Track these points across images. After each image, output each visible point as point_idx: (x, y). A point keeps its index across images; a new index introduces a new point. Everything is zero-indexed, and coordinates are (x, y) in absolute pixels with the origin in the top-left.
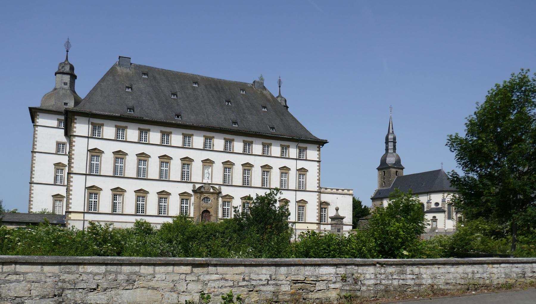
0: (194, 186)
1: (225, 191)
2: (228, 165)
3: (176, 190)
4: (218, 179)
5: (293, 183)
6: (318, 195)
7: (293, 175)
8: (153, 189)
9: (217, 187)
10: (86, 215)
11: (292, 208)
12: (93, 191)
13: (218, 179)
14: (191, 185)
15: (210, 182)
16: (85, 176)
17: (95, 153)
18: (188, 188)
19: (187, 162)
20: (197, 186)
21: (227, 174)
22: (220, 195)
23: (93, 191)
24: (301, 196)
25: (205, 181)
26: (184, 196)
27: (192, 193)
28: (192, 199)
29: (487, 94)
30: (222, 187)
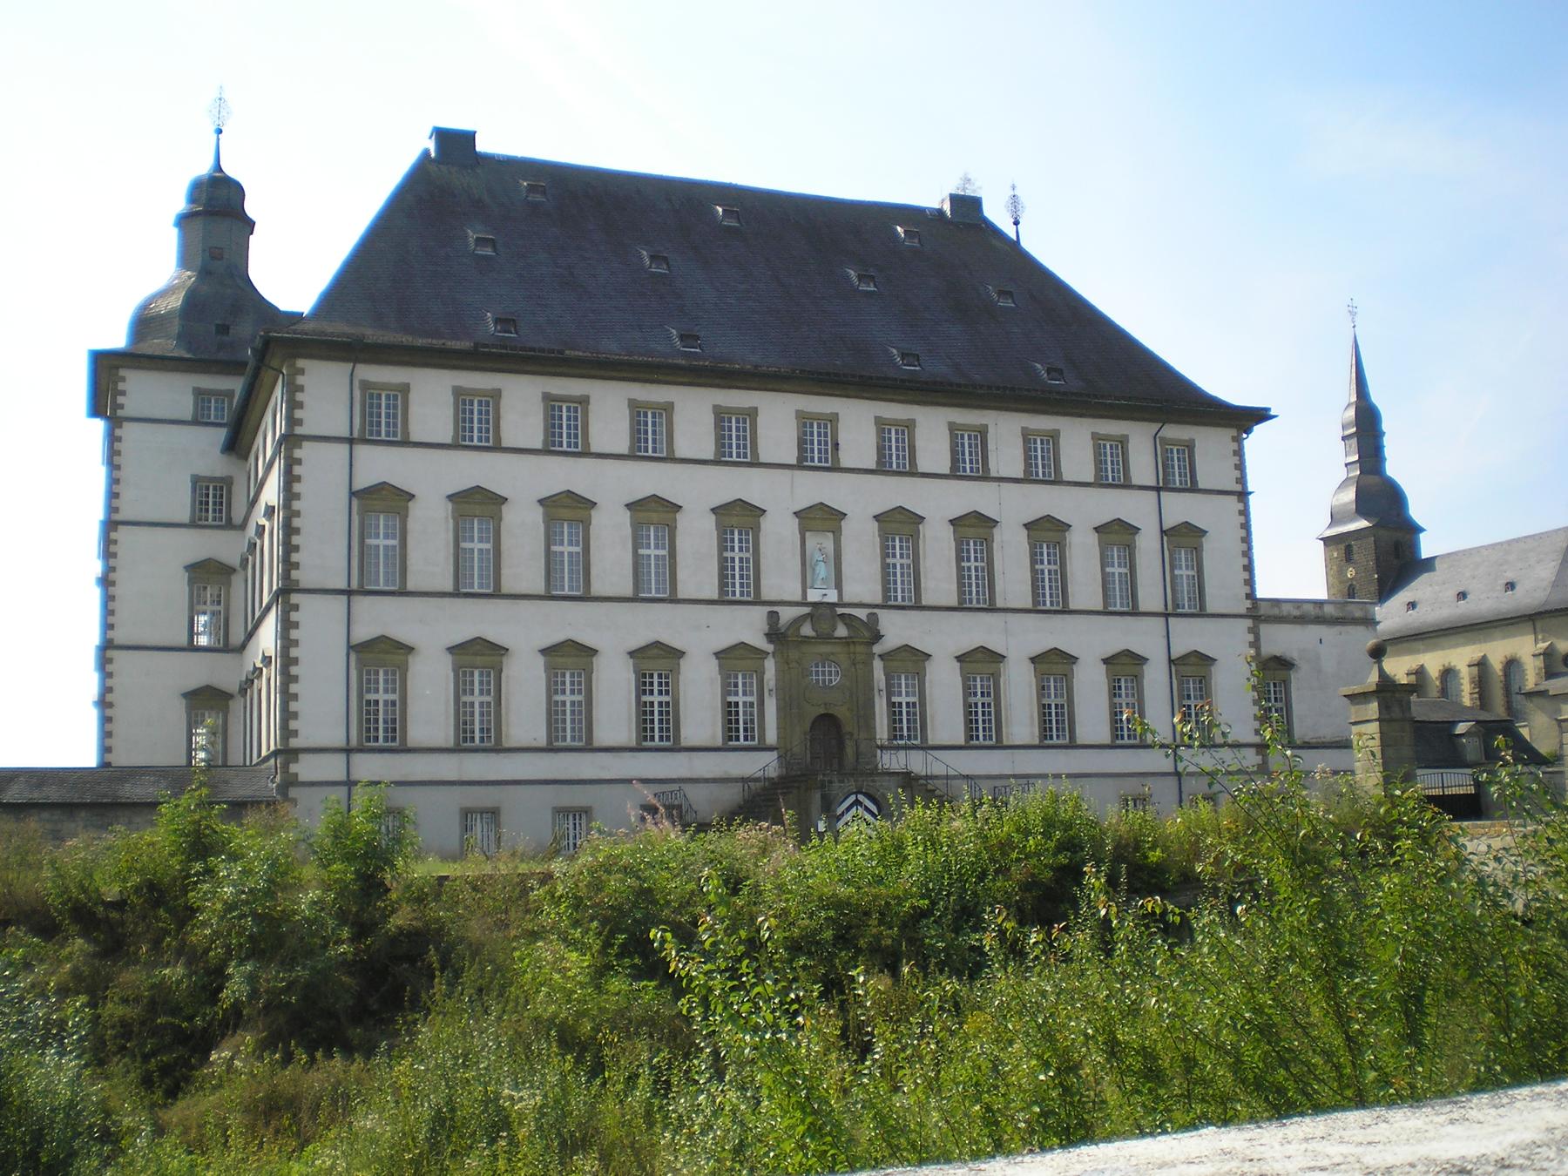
0: (773, 616)
1: (897, 629)
2: (899, 525)
3: (702, 635)
4: (862, 584)
5: (939, 582)
6: (1250, 630)
7: (938, 545)
8: (431, 630)
9: (862, 614)
10: (357, 758)
11: (944, 694)
12: (380, 657)
13: (862, 584)
14: (759, 615)
15: (832, 597)
16: (344, 598)
17: (569, 510)
18: (748, 626)
19: (738, 518)
20: (787, 614)
21: (737, 555)
22: (877, 649)
23: (380, 657)
24: (1190, 636)
25: (813, 596)
26: (733, 658)
27: (770, 648)
28: (770, 666)
29: (977, 184)
30: (883, 615)
